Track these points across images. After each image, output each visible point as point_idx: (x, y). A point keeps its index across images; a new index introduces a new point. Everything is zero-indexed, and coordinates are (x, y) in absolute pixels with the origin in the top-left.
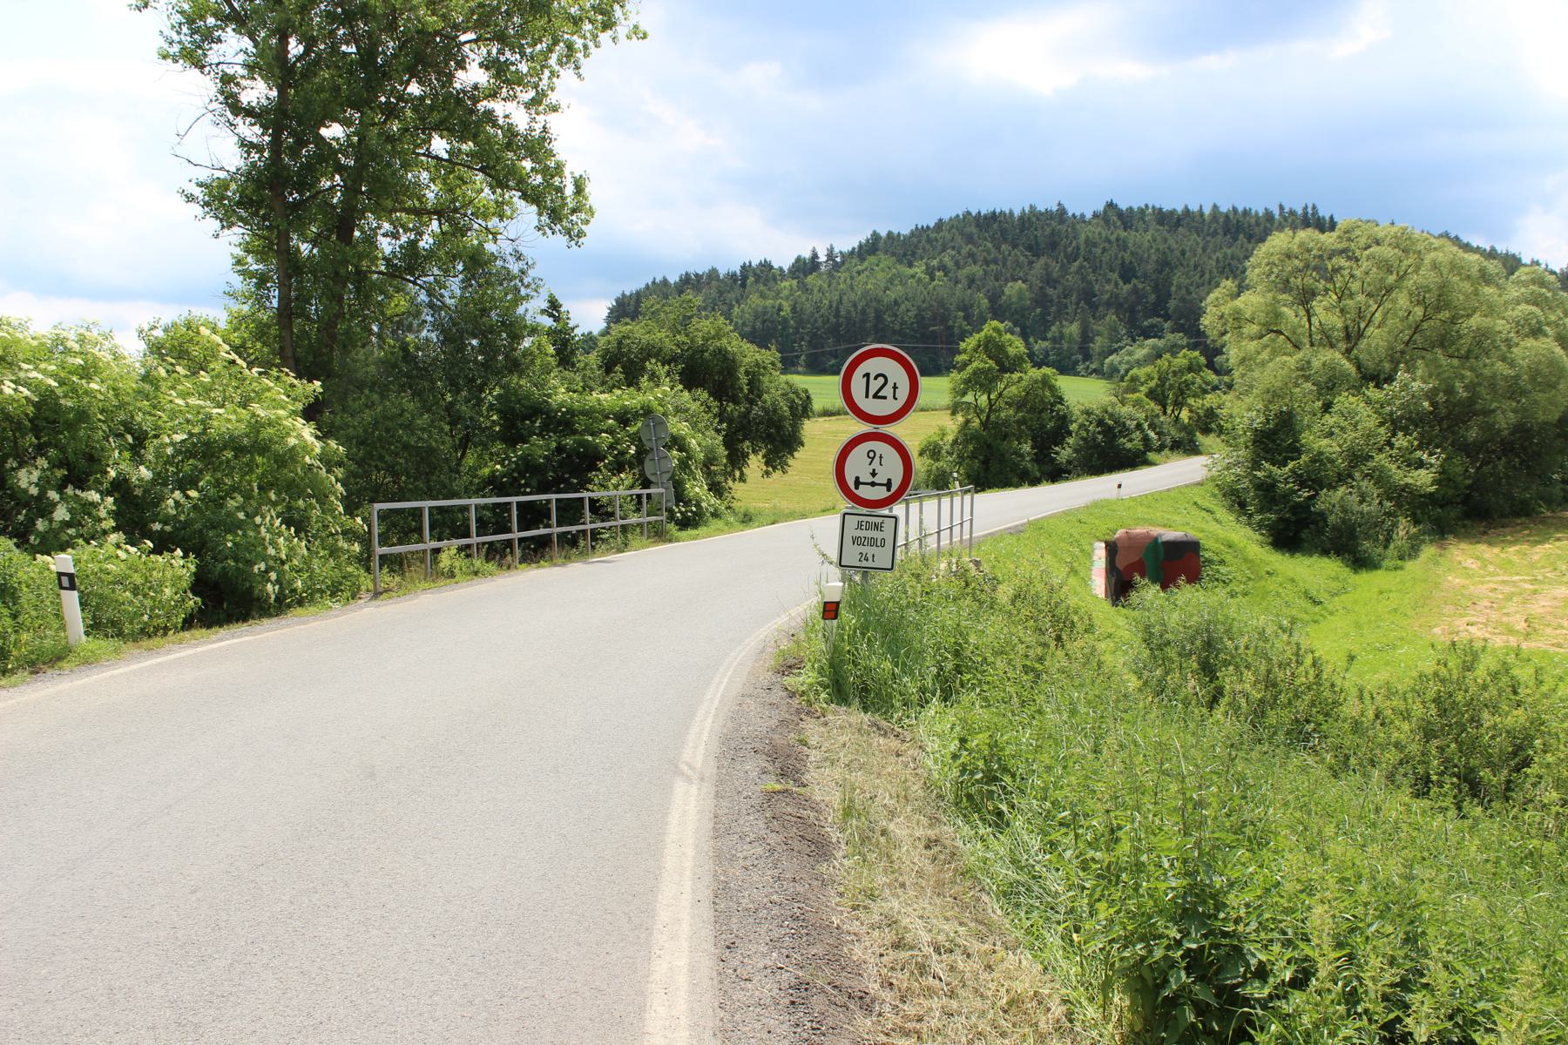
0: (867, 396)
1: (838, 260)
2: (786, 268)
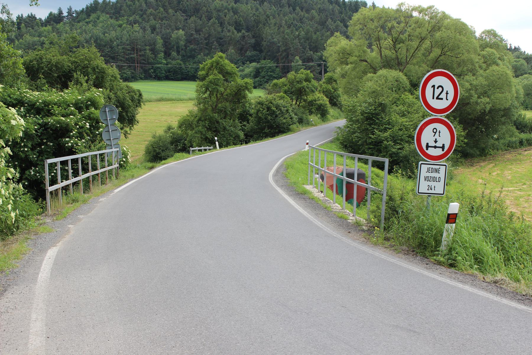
0: (433, 98)
1: (74, 15)
2: (43, 19)
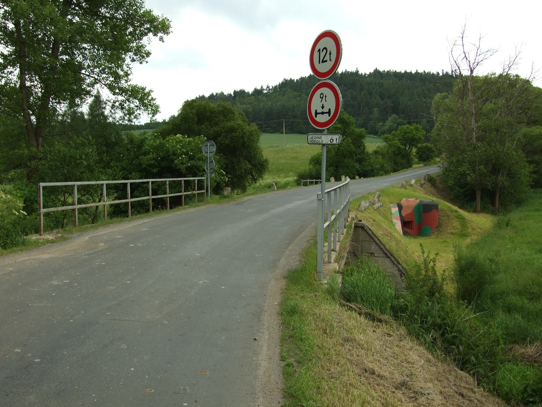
0: (319, 63)
